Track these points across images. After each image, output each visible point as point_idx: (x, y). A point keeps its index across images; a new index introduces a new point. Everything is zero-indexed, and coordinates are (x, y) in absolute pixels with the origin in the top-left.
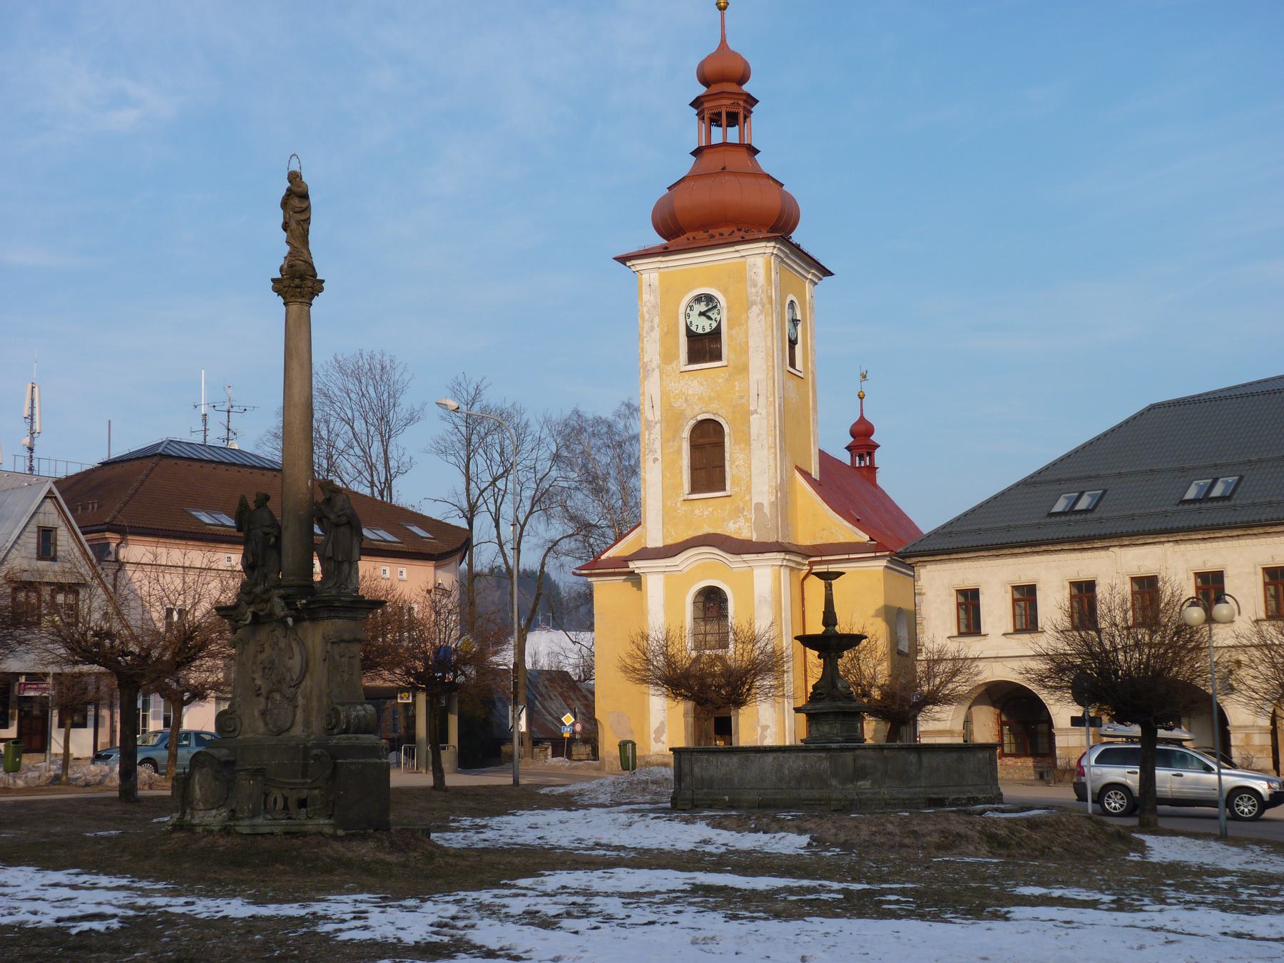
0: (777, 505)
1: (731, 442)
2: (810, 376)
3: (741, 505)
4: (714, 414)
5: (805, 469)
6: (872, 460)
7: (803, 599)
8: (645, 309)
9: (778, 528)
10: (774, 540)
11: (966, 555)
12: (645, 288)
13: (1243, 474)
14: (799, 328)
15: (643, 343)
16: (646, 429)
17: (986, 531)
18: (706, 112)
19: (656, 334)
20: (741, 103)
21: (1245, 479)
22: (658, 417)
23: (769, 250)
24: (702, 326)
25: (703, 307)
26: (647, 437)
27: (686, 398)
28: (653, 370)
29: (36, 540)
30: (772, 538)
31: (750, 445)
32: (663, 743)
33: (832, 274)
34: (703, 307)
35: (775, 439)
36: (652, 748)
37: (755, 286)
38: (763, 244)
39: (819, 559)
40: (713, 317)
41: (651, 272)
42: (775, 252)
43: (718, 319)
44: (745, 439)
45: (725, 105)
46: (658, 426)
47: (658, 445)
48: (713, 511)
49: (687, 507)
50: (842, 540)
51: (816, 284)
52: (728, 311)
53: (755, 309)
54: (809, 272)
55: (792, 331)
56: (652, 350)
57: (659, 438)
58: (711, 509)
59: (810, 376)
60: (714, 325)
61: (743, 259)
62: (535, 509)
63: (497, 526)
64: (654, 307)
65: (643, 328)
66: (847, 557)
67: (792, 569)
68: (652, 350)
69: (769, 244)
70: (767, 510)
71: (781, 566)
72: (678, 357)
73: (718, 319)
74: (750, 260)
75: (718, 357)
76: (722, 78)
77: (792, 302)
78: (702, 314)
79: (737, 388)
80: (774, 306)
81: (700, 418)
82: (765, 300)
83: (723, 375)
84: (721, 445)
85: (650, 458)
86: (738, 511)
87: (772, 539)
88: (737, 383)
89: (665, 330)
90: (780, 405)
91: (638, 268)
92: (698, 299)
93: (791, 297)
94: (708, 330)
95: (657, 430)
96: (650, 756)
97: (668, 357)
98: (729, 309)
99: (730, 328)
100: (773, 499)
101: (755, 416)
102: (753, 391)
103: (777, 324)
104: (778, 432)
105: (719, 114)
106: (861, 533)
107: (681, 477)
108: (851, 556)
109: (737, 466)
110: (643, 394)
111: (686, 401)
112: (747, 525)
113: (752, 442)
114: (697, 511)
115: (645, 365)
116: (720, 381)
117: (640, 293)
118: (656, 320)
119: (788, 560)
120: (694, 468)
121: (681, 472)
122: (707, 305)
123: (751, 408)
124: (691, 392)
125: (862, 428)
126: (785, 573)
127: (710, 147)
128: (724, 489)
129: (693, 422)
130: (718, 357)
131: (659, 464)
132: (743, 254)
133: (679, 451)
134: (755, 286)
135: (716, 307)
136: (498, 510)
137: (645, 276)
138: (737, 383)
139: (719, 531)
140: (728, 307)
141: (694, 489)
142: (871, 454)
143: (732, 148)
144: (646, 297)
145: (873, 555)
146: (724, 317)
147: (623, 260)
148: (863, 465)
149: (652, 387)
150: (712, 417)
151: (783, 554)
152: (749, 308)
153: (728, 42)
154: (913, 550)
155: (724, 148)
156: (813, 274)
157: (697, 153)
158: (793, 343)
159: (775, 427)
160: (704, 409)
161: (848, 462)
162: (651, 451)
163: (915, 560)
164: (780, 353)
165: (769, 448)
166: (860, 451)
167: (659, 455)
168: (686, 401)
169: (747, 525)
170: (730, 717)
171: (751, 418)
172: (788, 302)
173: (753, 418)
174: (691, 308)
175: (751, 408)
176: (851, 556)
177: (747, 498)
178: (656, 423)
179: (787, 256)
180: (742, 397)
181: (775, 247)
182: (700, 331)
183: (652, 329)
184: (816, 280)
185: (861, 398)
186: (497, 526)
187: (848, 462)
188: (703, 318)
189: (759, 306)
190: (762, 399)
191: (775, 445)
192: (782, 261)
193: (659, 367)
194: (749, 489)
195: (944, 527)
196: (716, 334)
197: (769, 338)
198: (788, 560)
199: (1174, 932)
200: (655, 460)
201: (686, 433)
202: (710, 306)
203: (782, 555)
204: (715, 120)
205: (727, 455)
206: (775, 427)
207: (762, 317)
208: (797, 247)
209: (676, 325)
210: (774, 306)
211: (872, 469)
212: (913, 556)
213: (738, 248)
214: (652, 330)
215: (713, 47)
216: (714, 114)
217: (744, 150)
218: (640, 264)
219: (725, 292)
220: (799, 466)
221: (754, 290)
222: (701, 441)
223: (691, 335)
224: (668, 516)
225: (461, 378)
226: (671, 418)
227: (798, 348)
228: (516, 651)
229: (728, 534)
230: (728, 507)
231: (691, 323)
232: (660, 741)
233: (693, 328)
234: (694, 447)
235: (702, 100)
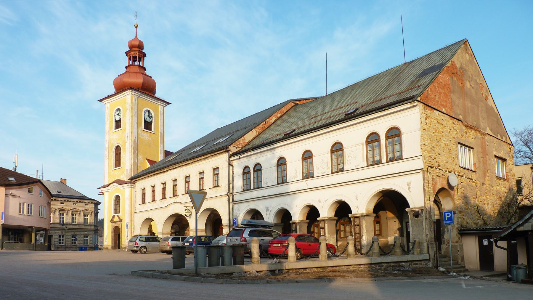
20: (137, 53)
24: (118, 118)
29: (186, 262)
33: (171, 104)
53: (128, 111)
54: (159, 102)
60: (151, 121)
61: (125, 97)
78: (118, 114)
81: (116, 146)
97: (110, 128)
99: (123, 118)
101: (127, 143)
132: (125, 95)
147: (101, 101)
156: (160, 103)
157: (126, 68)
173: (126, 144)
182: (117, 120)
199: (63, 260)
213: (123, 93)
215: (134, 37)
218: (105, 101)
221: (128, 106)
228: (442, 240)
233: (116, 119)
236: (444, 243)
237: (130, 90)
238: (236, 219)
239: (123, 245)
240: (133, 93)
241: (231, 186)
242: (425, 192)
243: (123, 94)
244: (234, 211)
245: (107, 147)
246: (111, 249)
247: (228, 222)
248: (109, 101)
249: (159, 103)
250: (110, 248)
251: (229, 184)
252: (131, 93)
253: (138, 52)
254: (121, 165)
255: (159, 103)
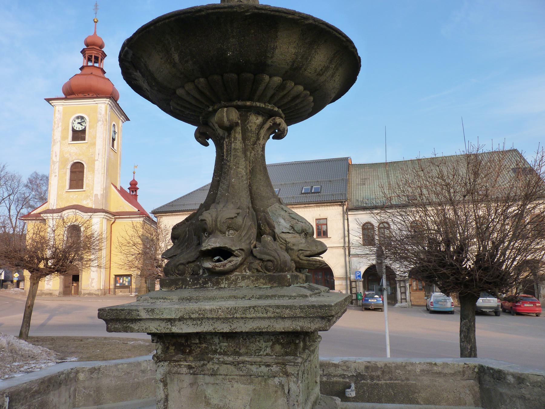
0: (103, 195)
1: (87, 171)
2: (119, 153)
3: (89, 194)
4: (81, 160)
5: (115, 185)
6: (136, 193)
7: (111, 231)
8: (56, 119)
9: (103, 204)
10: (101, 208)
11: (178, 213)
12: (57, 112)
13: (280, 188)
14: (116, 135)
15: (54, 132)
16: (53, 164)
17: (187, 205)
18: (86, 54)
19: (60, 129)
20: (100, 54)
21: (281, 189)
22: (58, 159)
23: (107, 102)
24: (79, 127)
25: (79, 121)
26: (53, 167)
27: (70, 153)
28: (57, 142)
30: (100, 207)
31: (94, 172)
32: (50, 285)
33: (121, 186)
34: (79, 121)
35: (104, 171)
36: (45, 287)
37: (101, 114)
38: (105, 99)
39: (118, 217)
40: (83, 125)
41: (60, 106)
42: (109, 103)
43: (85, 126)
44: (93, 170)
45: (94, 53)
46: (58, 163)
47: (57, 171)
48: (78, 196)
49: (67, 194)
50: (127, 211)
51: (123, 122)
52: (89, 123)
53: (100, 123)
54: (121, 117)
55: (114, 135)
56: (57, 135)
57: (58, 167)
58: (77, 196)
59: (119, 153)
60: (83, 128)
61: (97, 105)
62: (23, 207)
63: (9, 212)
64: (60, 119)
65: (54, 127)
66: (129, 216)
67: (108, 220)
68: (57, 135)
69: (107, 100)
70: (99, 197)
71: (104, 218)
72: (68, 138)
73: (85, 126)
74: (99, 105)
75: (84, 139)
76: (94, 44)
77: (114, 125)
79: (91, 151)
80: (107, 122)
81: (75, 161)
82: (104, 120)
83: (85, 146)
84: (82, 172)
85: (53, 175)
86: (88, 197)
87: (100, 208)
88: (91, 149)
89: (64, 128)
90: (107, 159)
91: (54, 104)
92: (78, 118)
93: (114, 123)
94: (81, 129)
95: (57, 165)
96: (44, 290)
97: (64, 138)
98: (90, 122)
99: (90, 129)
100: (102, 193)
101: (97, 162)
102: (97, 152)
103: (108, 129)
104: (106, 169)
105: (91, 56)
106: (135, 208)
107: (66, 183)
108: (131, 216)
109: (88, 180)
110: (53, 151)
111: (70, 155)
112: (91, 202)
113: (95, 171)
114: (71, 196)
115: (54, 140)
116: (84, 148)
117: (55, 113)
118: (60, 124)
119: (107, 216)
120: (71, 180)
121: (66, 181)
122: (81, 120)
123: (96, 159)
124: (72, 151)
125: (134, 182)
126: (105, 221)
127: (87, 66)
128: (83, 188)
129: (72, 163)
130: (84, 139)
131: (57, 177)
133: (65, 173)
134: (101, 114)
135: (85, 121)
136: (10, 207)
137: (57, 108)
138: (91, 149)
139: (79, 204)
140: (89, 121)
141: (70, 188)
142: (136, 191)
143: (96, 68)
144: (57, 115)
145: (139, 216)
146: (87, 125)
147: (48, 100)
148: (133, 194)
149: (56, 149)
150: (80, 161)
151: (104, 213)
152: (98, 122)
153: (97, 33)
154: (158, 211)
155: (92, 67)
156: (123, 118)
157: (81, 69)
158: (114, 140)
159: (105, 166)
160: (77, 158)
161: (129, 192)
162: (54, 172)
163: (158, 215)
164: (109, 140)
165: (102, 174)
166: (132, 190)
167: (57, 174)
168: (70, 155)
169: (91, 202)
170: (79, 275)
171: (95, 162)
172: (112, 125)
173: (96, 163)
174: (75, 121)
175: (96, 159)
176: (131, 216)
177: (92, 192)
178: (57, 162)
179: (114, 107)
180: (92, 155)
181: (109, 101)
182: (77, 129)
183: (58, 127)
184: (124, 121)
185: (134, 173)
186: (9, 212)
187: (129, 192)
188: (79, 125)
189: (102, 122)
190: (100, 156)
191: (104, 172)
192: (112, 108)
193: (60, 141)
194: (93, 189)
195: (169, 203)
196: (84, 131)
197: (105, 134)
198: (107, 216)
200: (55, 176)
201: (69, 167)
202: (82, 121)
203: (104, 214)
204: (89, 60)
205: (85, 176)
206: (105, 166)
207: (102, 126)
208: (118, 104)
209: (68, 126)
210: (107, 122)
211: (136, 196)
212: (157, 213)
214: (58, 128)
215: (92, 34)
216: (89, 56)
217: (100, 70)
218: (54, 103)
219: (88, 116)
220: (113, 183)
221: (100, 116)
222: (75, 170)
223: (74, 131)
224: (59, 197)
225: (8, 172)
226: (63, 160)
227: (115, 142)
229: (83, 205)
230: (84, 195)
231: (74, 126)
232: (49, 284)
233: (75, 128)
234: (72, 172)
235: (85, 50)
236: (541, 297)
237: (107, 99)
238: (356, 272)
239: (83, 290)
240: (109, 103)
241: (347, 239)
242: (76, 209)
243: (94, 101)
244: (353, 264)
245: (55, 160)
246: (59, 294)
247: (345, 274)
248: (64, 104)
249: (121, 118)
250: (57, 293)
251: (344, 237)
252: (107, 102)
253: (101, 53)
254: (84, 187)
255: (121, 118)
